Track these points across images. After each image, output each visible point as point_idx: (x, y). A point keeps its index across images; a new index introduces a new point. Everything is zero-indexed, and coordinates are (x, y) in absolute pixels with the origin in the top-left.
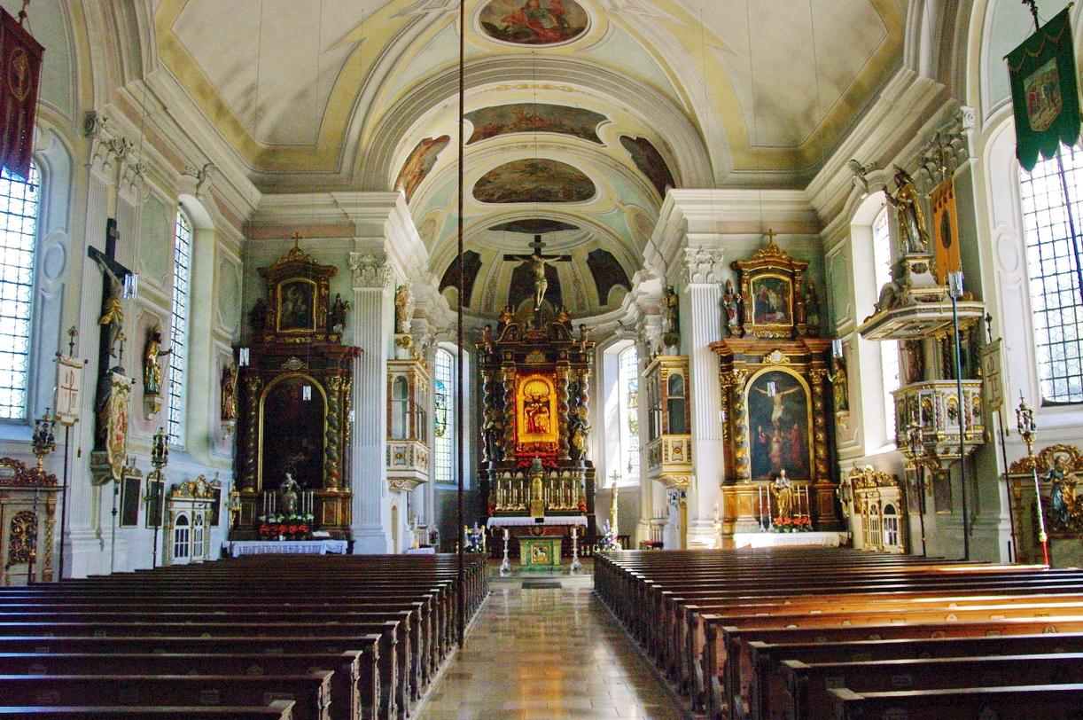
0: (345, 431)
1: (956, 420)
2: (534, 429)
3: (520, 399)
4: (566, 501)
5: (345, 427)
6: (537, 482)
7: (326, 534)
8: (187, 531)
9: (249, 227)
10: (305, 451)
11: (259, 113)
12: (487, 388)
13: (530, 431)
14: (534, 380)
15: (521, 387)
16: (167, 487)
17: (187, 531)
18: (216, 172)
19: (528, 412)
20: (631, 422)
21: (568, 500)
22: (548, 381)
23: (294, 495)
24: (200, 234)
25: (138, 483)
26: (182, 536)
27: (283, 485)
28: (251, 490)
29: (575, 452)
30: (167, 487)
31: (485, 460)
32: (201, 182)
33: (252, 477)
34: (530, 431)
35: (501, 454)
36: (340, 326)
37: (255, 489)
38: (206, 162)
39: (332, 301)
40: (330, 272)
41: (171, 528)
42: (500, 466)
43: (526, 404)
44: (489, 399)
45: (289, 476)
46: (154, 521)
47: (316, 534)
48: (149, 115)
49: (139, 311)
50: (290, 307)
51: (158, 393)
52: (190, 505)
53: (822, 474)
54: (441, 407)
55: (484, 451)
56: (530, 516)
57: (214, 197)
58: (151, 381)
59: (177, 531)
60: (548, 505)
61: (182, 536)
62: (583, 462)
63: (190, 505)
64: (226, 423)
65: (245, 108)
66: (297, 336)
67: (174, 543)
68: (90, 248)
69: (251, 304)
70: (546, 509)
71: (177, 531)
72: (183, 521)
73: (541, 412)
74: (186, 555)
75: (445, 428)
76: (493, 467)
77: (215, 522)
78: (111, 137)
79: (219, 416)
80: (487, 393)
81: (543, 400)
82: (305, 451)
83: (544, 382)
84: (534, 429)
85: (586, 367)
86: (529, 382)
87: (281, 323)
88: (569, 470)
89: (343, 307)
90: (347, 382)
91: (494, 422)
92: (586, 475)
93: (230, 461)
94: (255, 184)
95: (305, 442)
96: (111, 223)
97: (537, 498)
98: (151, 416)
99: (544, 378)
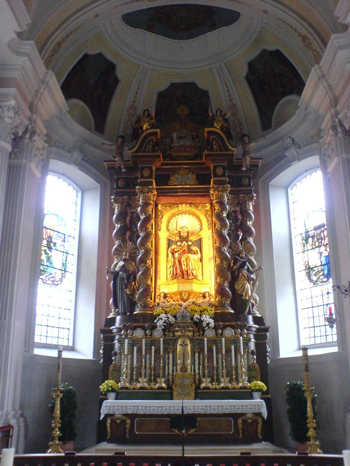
2: (182, 274)
3: (163, 235)
4: (229, 374)
6: (184, 345)
12: (118, 220)
13: (175, 276)
14: (182, 213)
15: (164, 220)
16: (160, 317)
19: (173, 254)
20: (309, 269)
21: (232, 374)
22: (198, 213)
29: (240, 303)
30: (160, 317)
31: (111, 316)
34: (175, 276)
35: (132, 305)
42: (132, 322)
43: (170, 243)
44: (121, 233)
53: (245, 373)
54: (58, 247)
55: (258, 298)
56: (172, 399)
60: (200, 382)
62: (250, 317)
70: (198, 387)
73: (190, 251)
75: (63, 276)
76: (122, 321)
80: (117, 226)
81: (193, 238)
83: (194, 214)
84: (182, 274)
85: (250, 192)
86: (174, 215)
88: (233, 327)
91: (125, 260)
92: (256, 337)
97: (184, 369)
99: (195, 210)
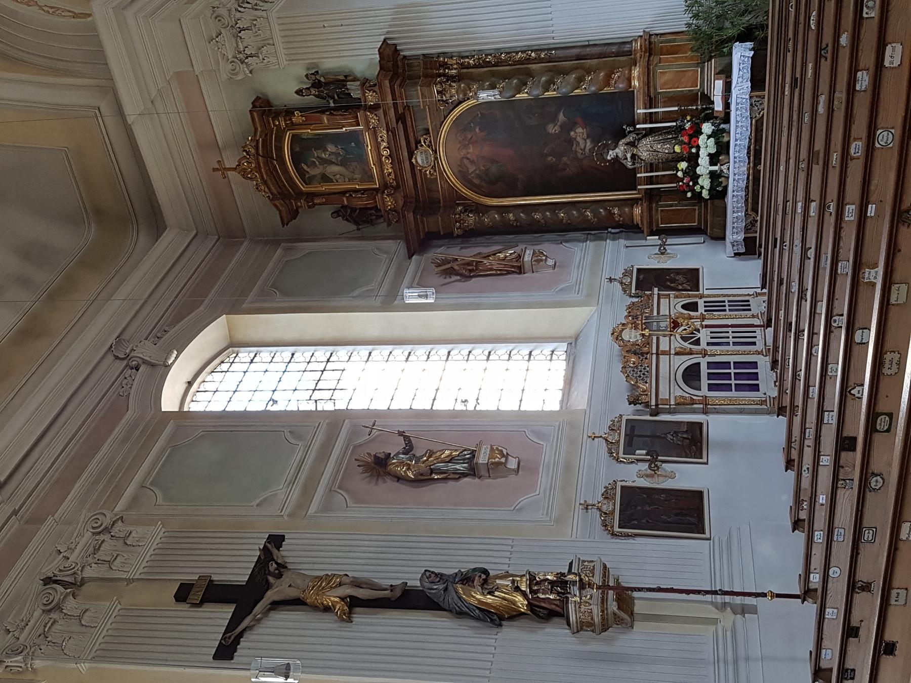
0: (529, 60)
1: (792, 474)
5: (521, 62)
7: (719, 84)
8: (710, 365)
9: (230, 234)
10: (568, 127)
11: (35, 254)
17: (710, 365)
18: (126, 336)
23: (647, 142)
24: (240, 336)
25: (629, 493)
26: (720, 376)
27: (629, 165)
28: (637, 211)
32: (145, 362)
33: (616, 211)
36: (350, 85)
37: (633, 202)
38: (110, 358)
39: (311, 99)
40: (264, 108)
41: (705, 401)
45: (611, 155)
46: (692, 443)
47: (718, 106)
48: (15, 513)
49: (339, 499)
50: (335, 169)
51: (473, 453)
52: (664, 359)
57: (173, 324)
58: (451, 466)
59: (711, 387)
61: (720, 376)
63: (664, 359)
64: (527, 266)
65: (24, 282)
66: (380, 156)
67: (733, 394)
68: (216, 657)
69: (343, 225)
71: (711, 387)
72: (691, 375)
74: (754, 365)
77: (692, 277)
78: (88, 535)
79: (514, 279)
82: (568, 127)
87: (362, 181)
89: (317, 84)
90: (445, 65)
93: (591, 245)
94: (158, 237)
95: (552, 129)
96: (183, 594)
98: (512, 464)
